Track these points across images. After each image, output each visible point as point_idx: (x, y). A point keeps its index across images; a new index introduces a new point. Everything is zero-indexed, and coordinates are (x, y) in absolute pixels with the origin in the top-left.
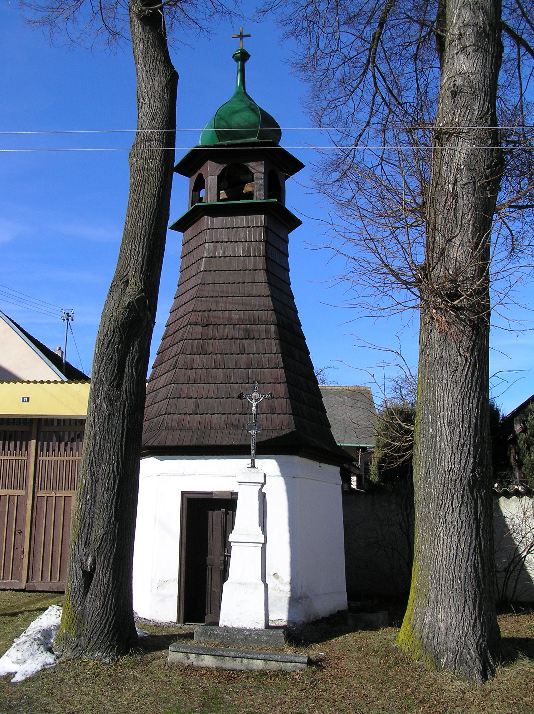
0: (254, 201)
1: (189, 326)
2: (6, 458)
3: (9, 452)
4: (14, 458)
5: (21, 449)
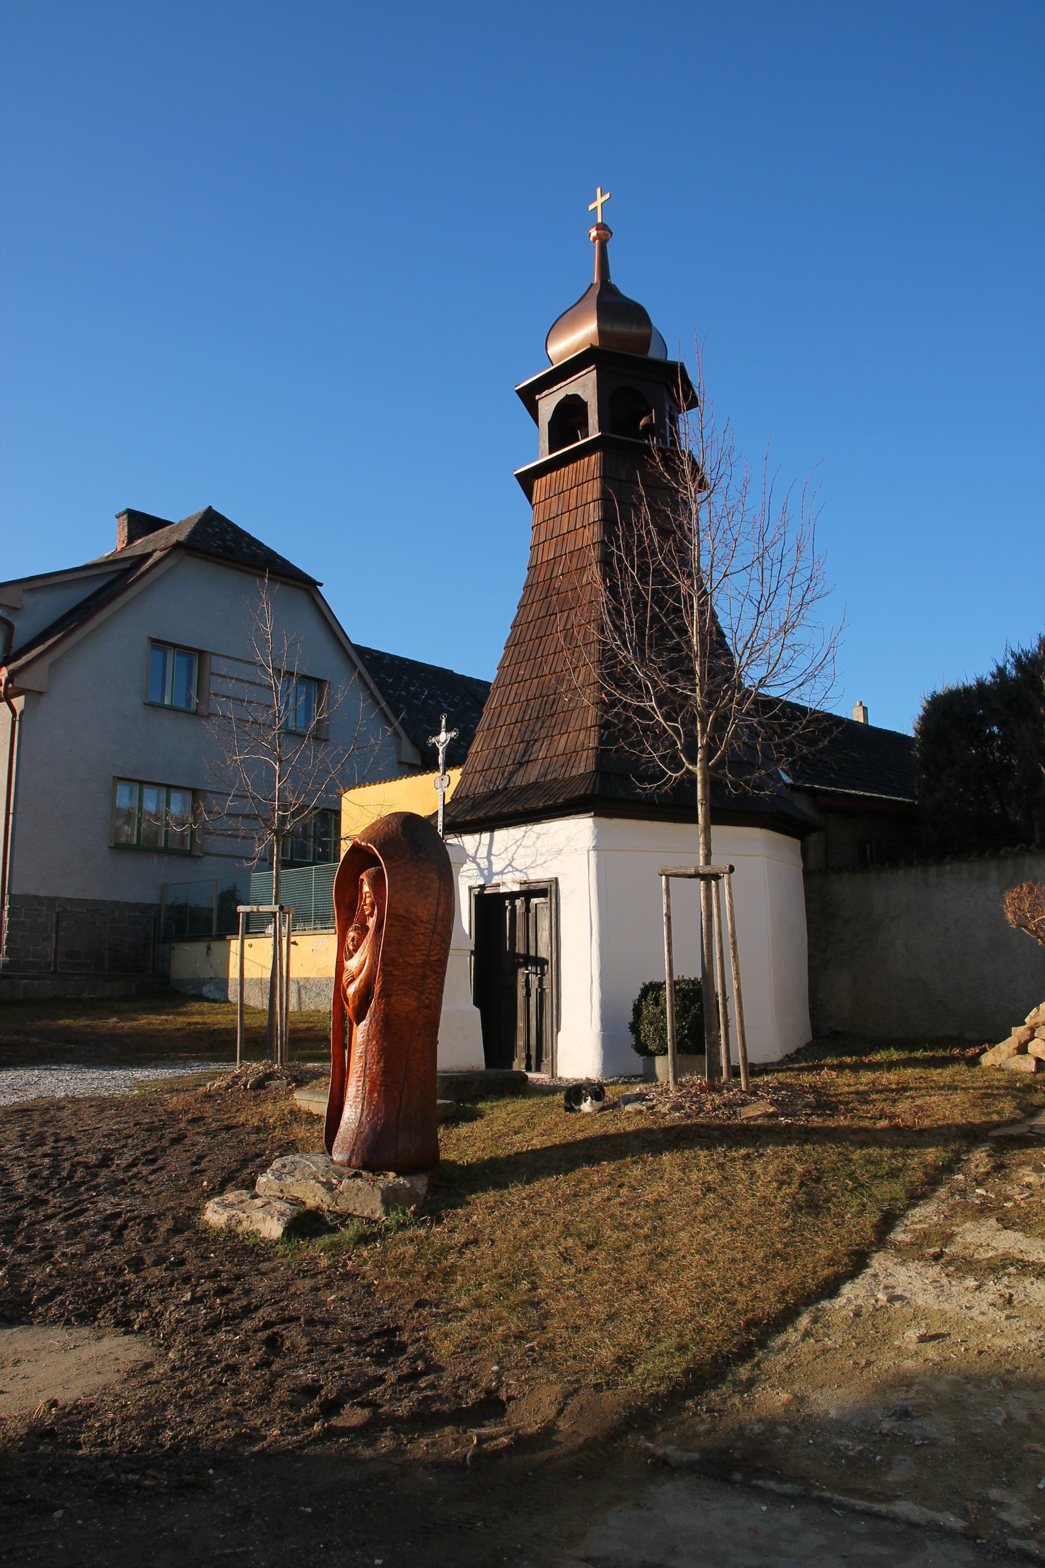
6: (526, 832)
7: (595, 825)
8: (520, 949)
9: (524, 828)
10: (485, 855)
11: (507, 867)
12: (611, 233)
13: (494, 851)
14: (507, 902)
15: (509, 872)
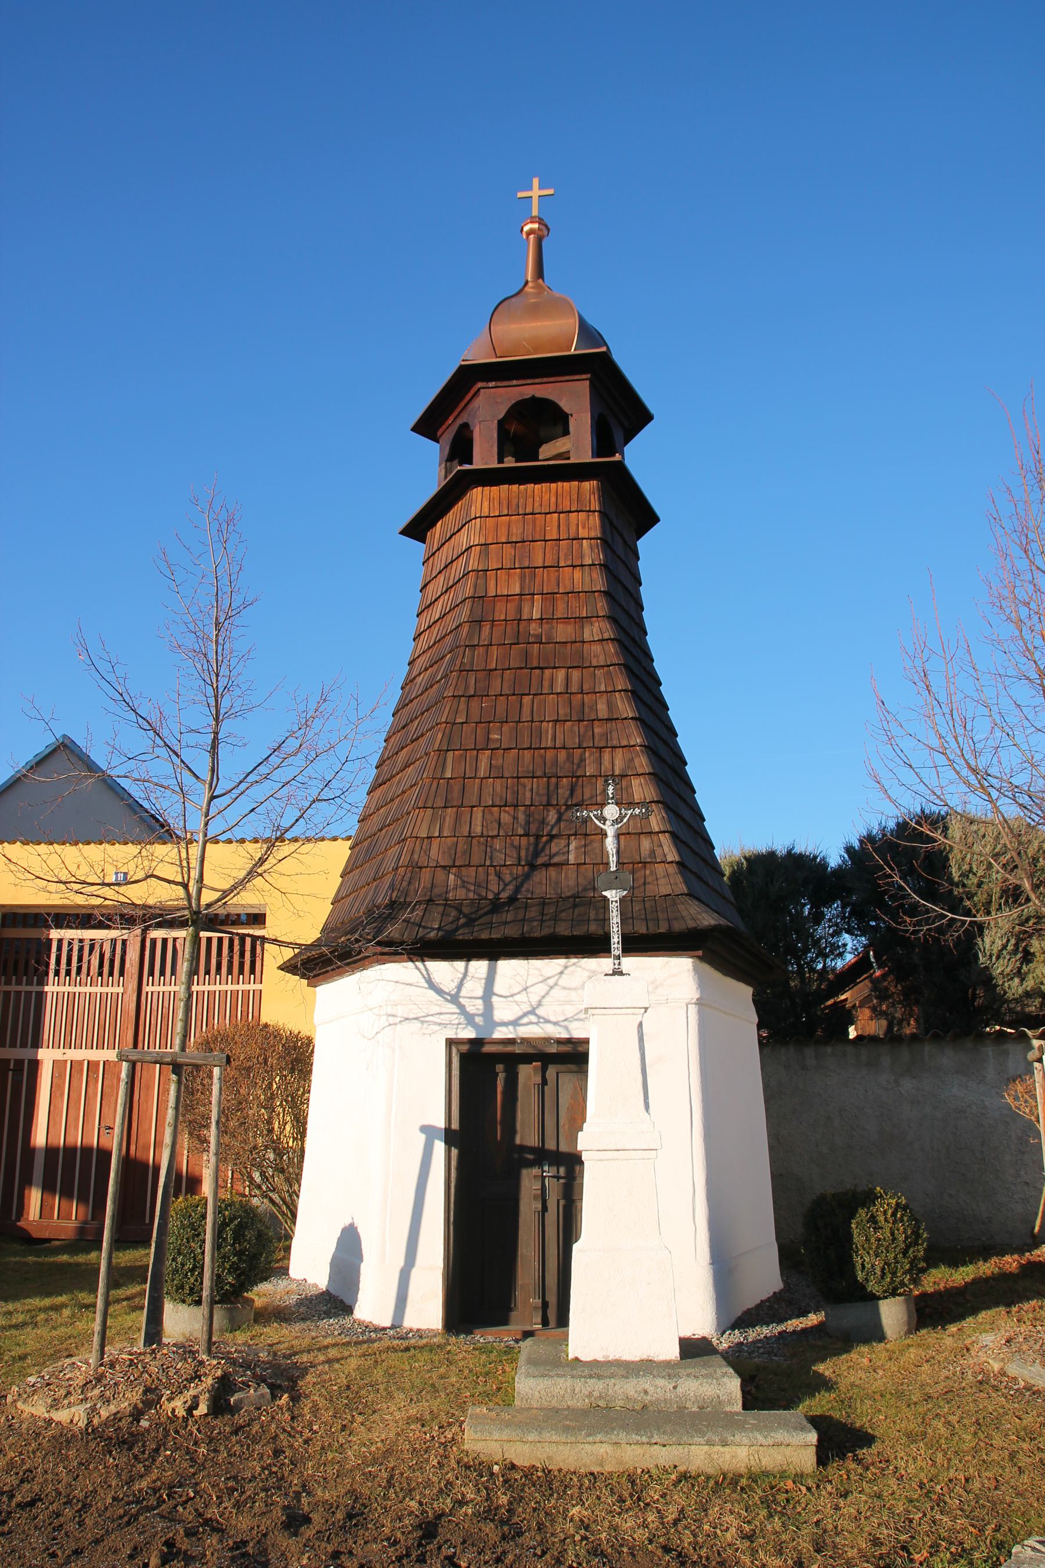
0: (572, 461)
1: (417, 811)
2: (83, 989)
3: (89, 978)
4: (99, 989)
5: (111, 974)
6: (566, 967)
7: (37, 1056)
8: (527, 1135)
9: (560, 962)
10: (480, 992)
11: (525, 1015)
12: (548, 230)
13: (498, 988)
14: (500, 1068)
15: (531, 1023)
